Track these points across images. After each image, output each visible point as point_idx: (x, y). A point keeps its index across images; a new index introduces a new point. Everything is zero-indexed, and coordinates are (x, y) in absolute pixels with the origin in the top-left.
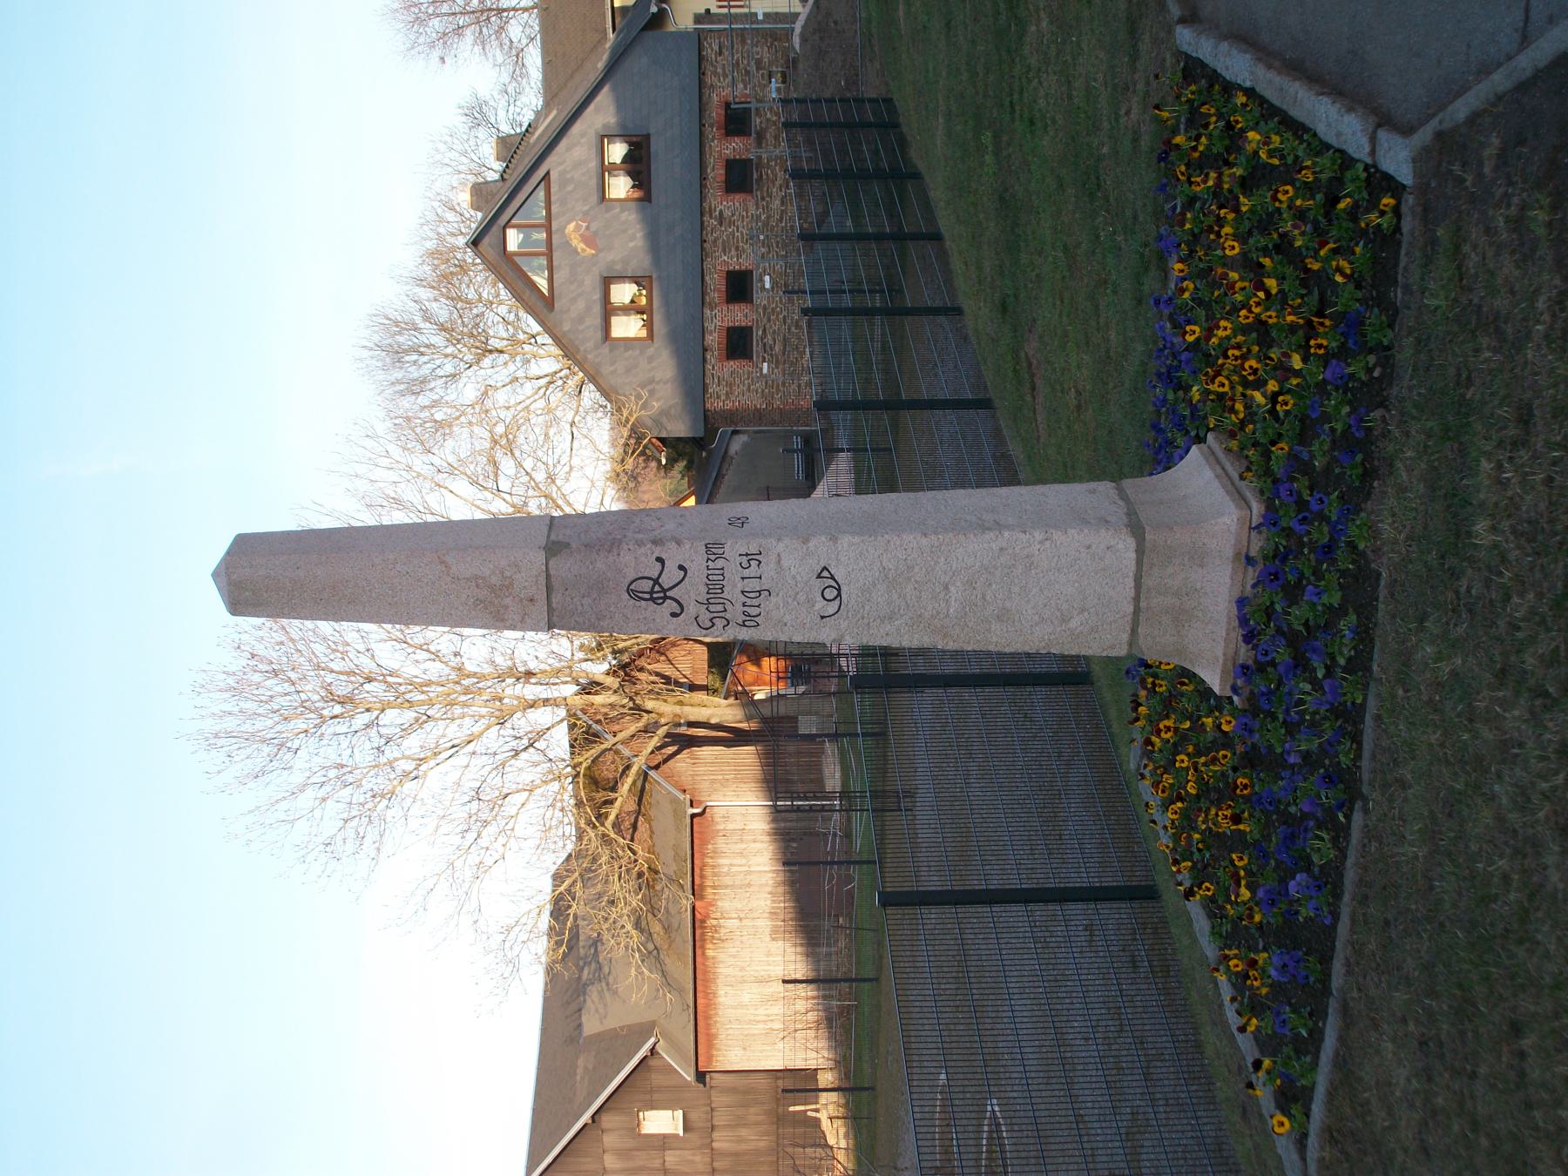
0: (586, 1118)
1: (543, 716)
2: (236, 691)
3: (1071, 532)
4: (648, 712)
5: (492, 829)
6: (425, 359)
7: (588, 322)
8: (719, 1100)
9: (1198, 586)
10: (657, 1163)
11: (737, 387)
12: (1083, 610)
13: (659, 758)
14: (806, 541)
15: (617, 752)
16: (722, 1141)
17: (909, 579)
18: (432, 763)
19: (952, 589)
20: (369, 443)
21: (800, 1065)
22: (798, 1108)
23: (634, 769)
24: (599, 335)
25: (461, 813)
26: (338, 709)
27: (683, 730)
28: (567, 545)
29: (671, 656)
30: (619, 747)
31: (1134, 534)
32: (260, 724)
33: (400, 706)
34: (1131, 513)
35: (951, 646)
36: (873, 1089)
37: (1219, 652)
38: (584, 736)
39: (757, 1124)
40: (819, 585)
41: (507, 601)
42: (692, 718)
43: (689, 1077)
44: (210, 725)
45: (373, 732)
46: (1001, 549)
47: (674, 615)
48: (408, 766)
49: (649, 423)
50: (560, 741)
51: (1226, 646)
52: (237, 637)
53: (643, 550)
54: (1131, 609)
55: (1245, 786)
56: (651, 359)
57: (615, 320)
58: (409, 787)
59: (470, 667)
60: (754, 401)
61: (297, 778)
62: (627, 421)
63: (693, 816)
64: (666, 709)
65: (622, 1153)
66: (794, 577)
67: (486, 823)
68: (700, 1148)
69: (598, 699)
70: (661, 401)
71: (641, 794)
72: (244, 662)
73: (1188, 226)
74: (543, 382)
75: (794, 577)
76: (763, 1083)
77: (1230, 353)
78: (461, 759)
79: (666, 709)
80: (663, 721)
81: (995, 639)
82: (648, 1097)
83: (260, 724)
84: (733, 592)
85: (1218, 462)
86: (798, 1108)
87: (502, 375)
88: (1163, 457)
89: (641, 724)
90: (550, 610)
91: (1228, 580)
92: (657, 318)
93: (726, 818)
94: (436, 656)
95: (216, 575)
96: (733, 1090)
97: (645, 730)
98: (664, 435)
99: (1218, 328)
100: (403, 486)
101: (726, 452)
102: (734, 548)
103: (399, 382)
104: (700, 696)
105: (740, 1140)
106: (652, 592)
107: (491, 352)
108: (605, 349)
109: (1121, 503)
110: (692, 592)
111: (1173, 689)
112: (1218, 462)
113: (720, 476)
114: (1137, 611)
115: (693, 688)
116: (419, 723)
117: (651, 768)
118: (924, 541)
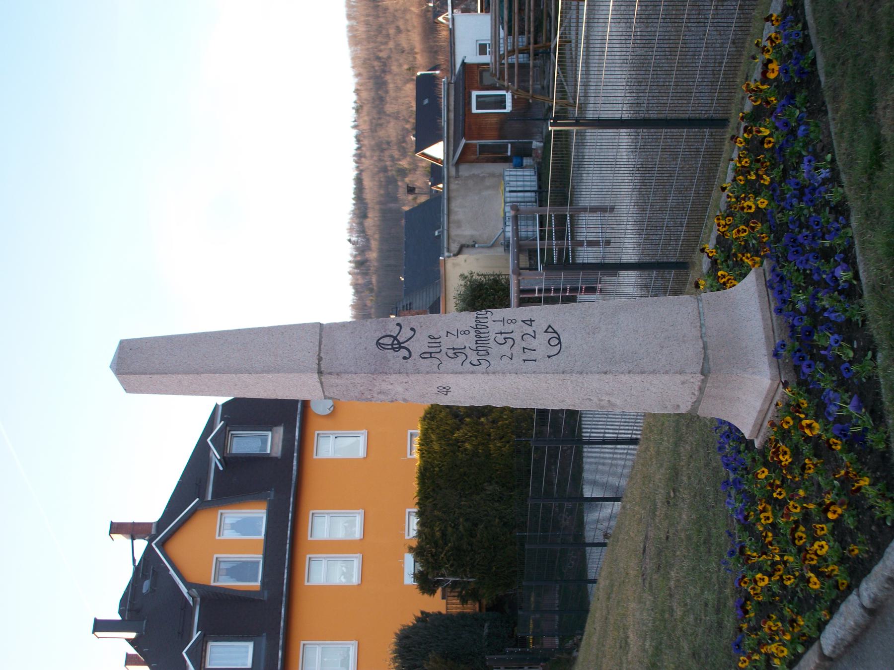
36: (608, 243)
47: (405, 358)
106: (392, 344)
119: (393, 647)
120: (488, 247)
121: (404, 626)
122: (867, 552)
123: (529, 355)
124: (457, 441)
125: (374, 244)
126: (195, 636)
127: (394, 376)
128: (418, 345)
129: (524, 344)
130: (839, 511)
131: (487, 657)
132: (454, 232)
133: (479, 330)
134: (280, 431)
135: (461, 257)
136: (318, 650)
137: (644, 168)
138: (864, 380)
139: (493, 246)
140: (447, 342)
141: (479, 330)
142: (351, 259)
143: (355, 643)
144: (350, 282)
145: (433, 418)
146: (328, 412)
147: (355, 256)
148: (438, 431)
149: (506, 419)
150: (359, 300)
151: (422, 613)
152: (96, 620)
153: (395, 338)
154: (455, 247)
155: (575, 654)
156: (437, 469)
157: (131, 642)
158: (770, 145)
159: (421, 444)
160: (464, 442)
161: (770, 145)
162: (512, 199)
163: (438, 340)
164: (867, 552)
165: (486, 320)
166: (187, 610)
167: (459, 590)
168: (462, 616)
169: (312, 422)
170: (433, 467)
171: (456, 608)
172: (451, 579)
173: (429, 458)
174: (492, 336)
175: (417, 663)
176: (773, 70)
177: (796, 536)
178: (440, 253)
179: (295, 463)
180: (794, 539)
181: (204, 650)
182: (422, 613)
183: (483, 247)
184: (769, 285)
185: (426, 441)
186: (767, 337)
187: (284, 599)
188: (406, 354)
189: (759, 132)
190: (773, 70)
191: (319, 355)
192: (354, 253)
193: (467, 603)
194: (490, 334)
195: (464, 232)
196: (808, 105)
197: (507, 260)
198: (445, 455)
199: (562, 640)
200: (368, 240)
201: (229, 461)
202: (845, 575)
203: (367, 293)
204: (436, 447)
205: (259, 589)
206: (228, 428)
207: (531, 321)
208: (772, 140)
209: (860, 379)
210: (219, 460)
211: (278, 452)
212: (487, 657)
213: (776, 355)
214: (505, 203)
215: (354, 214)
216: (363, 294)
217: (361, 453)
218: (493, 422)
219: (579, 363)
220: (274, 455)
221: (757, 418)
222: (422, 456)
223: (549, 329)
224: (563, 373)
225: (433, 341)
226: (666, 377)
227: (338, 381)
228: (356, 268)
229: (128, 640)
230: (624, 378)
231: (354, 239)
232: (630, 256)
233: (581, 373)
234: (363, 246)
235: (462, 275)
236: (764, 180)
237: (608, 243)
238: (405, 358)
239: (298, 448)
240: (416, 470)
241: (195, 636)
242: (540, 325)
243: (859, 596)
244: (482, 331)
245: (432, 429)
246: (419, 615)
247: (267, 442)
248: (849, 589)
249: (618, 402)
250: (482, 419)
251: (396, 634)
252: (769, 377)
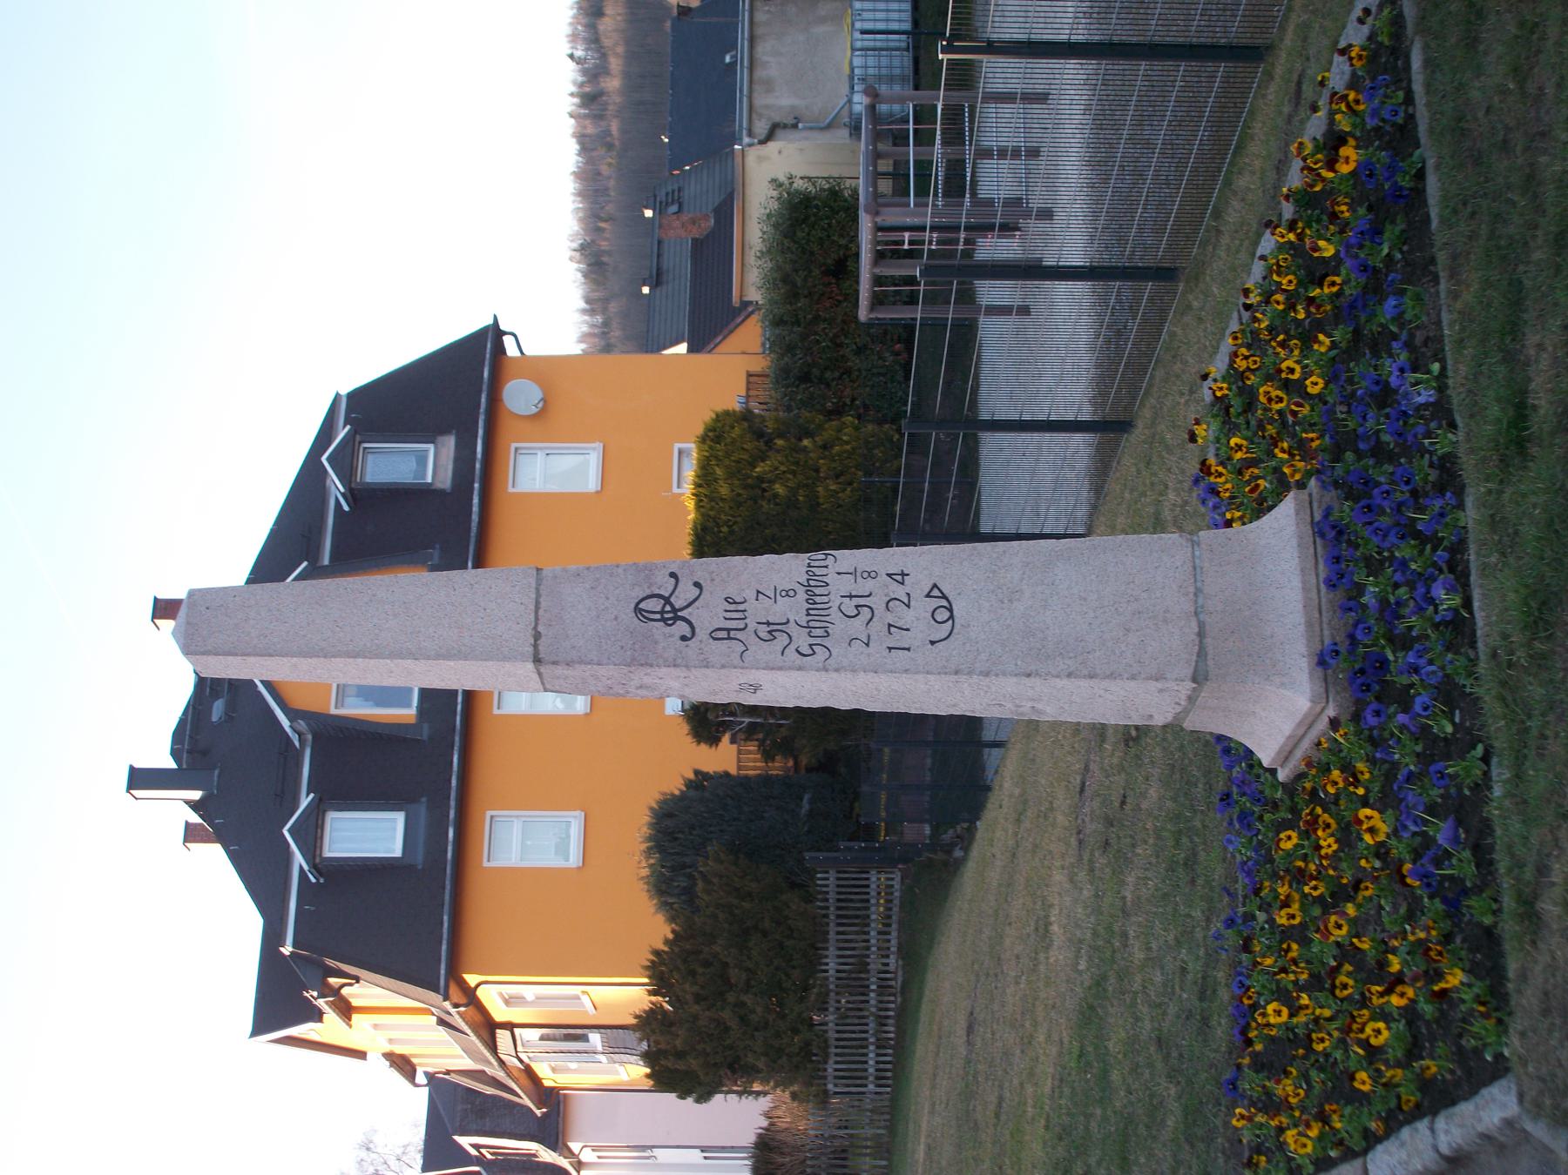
36: (1034, 153)
47: (684, 638)
106: (662, 612)
119: (646, 831)
120: (821, 129)
121: (664, 794)
122: (1452, 1072)
123: (898, 638)
124: (761, 479)
125: (615, 64)
126: (305, 801)
127: (664, 670)
128: (708, 615)
129: (890, 618)
130: (1410, 992)
131: (807, 855)
132: (761, 100)
133: (813, 587)
134: (449, 443)
135: (772, 146)
136: (517, 827)
137: (1104, 120)
138: (1467, 792)
139: (829, 127)
140: (758, 611)
141: (813, 587)
142: (573, 89)
143: (580, 814)
144: (571, 131)
145: (718, 439)
146: (534, 410)
147: (581, 85)
148: (727, 462)
149: (847, 443)
150: (586, 163)
151: (697, 772)
152: (132, 769)
153: (667, 600)
154: (761, 127)
155: (958, 853)
156: (725, 529)
157: (195, 806)
158: (1335, 289)
159: (697, 485)
160: (771, 482)
161: (1335, 289)
162: (867, 44)
163: (741, 607)
164: (1452, 1072)
165: (824, 571)
166: (289, 755)
167: (761, 736)
168: (766, 780)
169: (506, 428)
170: (718, 526)
171: (755, 768)
172: (747, 720)
173: (712, 509)
174: (836, 601)
175: (687, 860)
176: (1347, 158)
177: (1337, 983)
178: (734, 138)
179: (476, 500)
180: (1334, 986)
181: (319, 826)
182: (697, 772)
183: (811, 129)
184: (1319, 530)
185: (705, 478)
186: (1309, 624)
187: (457, 739)
188: (686, 630)
189: (1316, 249)
190: (1347, 158)
191: (535, 628)
192: (580, 79)
193: (773, 760)
194: (832, 597)
195: (779, 100)
196: (1405, 248)
197: (854, 152)
198: (740, 505)
199: (936, 830)
200: (604, 56)
201: (360, 496)
202: (1412, 1087)
203: (602, 151)
204: (724, 490)
205: (413, 721)
206: (358, 438)
207: (903, 574)
208: (1338, 280)
209: (1460, 788)
210: (343, 495)
211: (445, 481)
212: (807, 855)
213: (1321, 662)
214: (853, 49)
215: (580, 8)
216: (594, 154)
217: (592, 483)
218: (825, 447)
219: (983, 657)
220: (439, 485)
221: (1285, 744)
222: (698, 507)
223: (935, 592)
224: (956, 673)
225: (733, 607)
226: (1133, 684)
227: (569, 672)
228: (583, 105)
229: (187, 802)
230: (1059, 683)
231: (579, 53)
232: (1075, 254)
233: (987, 674)
234: (596, 66)
235: (774, 181)
236: (1320, 343)
237: (1034, 153)
238: (684, 638)
239: (480, 473)
240: (688, 528)
241: (305, 801)
242: (918, 584)
243: (1432, 1130)
244: (817, 591)
245: (716, 457)
246: (692, 776)
247: (424, 463)
248: (1417, 1113)
249: (1048, 709)
250: (806, 442)
251: (651, 809)
252: (1308, 695)
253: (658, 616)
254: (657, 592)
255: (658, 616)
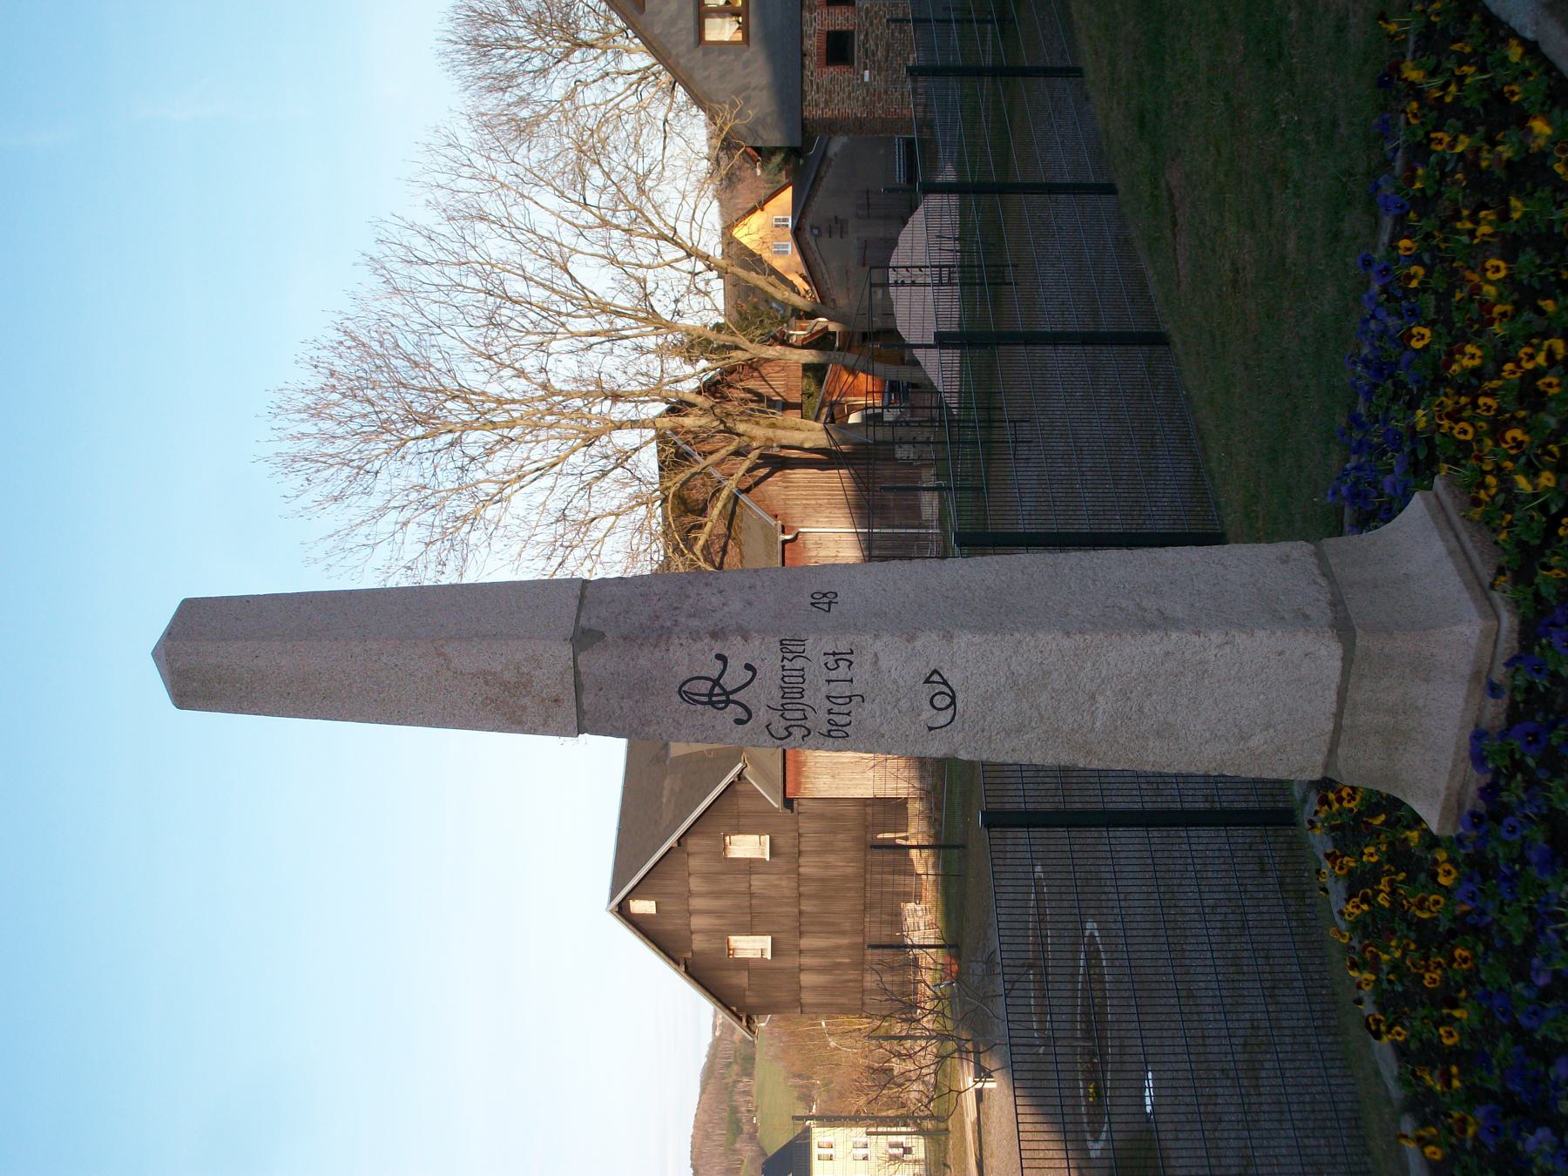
0: (671, 841)
1: (626, 439)
2: (316, 412)
3: (1260, 634)
4: (739, 435)
5: (579, 553)
6: (513, 52)
7: (681, 24)
8: (806, 826)
9: (1420, 703)
10: (743, 887)
11: (836, 94)
12: (1267, 727)
13: (750, 481)
14: (911, 639)
15: (709, 475)
16: (809, 867)
17: (1045, 686)
18: (516, 486)
19: (1100, 699)
20: (451, 152)
21: (891, 794)
22: (887, 835)
23: (725, 494)
24: (692, 39)
25: (545, 535)
26: (420, 430)
27: (775, 451)
28: (602, 636)
29: (764, 372)
30: (711, 470)
31: (1340, 638)
32: (340, 445)
33: (483, 427)
34: (1337, 603)
35: (1095, 765)
36: (962, 847)
37: (1442, 783)
38: (674, 457)
39: (845, 850)
40: (927, 690)
41: (526, 701)
42: (785, 442)
43: (776, 804)
44: (289, 447)
45: (457, 453)
46: (1167, 654)
47: (739, 722)
48: (492, 488)
49: (744, 131)
50: (648, 462)
51: (1452, 777)
52: (315, 353)
53: (699, 645)
54: (1331, 726)
55: (1465, 960)
56: (746, 65)
57: (709, 23)
58: (492, 512)
59: (558, 386)
60: (853, 108)
61: (376, 501)
62: (721, 130)
63: (785, 542)
64: (757, 432)
65: (707, 876)
66: (895, 682)
67: (572, 547)
68: (787, 872)
69: (689, 422)
70: (757, 106)
71: (731, 517)
72: (324, 380)
73: (1418, 185)
74: (635, 77)
75: (895, 682)
76: (852, 809)
77: (1481, 401)
78: (547, 481)
79: (757, 432)
80: (755, 444)
81: (1152, 758)
82: (734, 822)
83: (340, 445)
84: (815, 696)
85: (1451, 527)
86: (887, 835)
87: (592, 72)
88: (1374, 510)
89: (732, 448)
90: (580, 712)
91: (1461, 702)
92: (753, 22)
93: (819, 544)
94: (521, 373)
95: (156, 654)
96: (821, 817)
97: (737, 453)
98: (759, 144)
99: (1463, 354)
100: (485, 197)
101: (825, 153)
102: (817, 647)
103: (484, 77)
104: (793, 417)
105: (827, 866)
106: (710, 695)
107: (580, 46)
108: (699, 53)
109: (1322, 581)
110: (762, 696)
111: (1375, 817)
112: (1451, 527)
113: (817, 179)
114: (1338, 729)
115: (786, 406)
116: (505, 442)
117: (742, 491)
118: (1066, 643)
253: (705, 699)
254: (703, 674)
255: (705, 699)
